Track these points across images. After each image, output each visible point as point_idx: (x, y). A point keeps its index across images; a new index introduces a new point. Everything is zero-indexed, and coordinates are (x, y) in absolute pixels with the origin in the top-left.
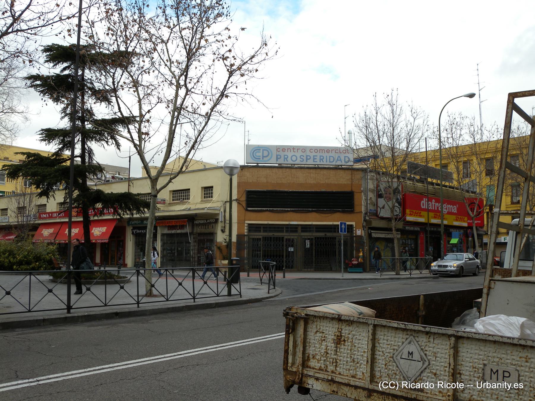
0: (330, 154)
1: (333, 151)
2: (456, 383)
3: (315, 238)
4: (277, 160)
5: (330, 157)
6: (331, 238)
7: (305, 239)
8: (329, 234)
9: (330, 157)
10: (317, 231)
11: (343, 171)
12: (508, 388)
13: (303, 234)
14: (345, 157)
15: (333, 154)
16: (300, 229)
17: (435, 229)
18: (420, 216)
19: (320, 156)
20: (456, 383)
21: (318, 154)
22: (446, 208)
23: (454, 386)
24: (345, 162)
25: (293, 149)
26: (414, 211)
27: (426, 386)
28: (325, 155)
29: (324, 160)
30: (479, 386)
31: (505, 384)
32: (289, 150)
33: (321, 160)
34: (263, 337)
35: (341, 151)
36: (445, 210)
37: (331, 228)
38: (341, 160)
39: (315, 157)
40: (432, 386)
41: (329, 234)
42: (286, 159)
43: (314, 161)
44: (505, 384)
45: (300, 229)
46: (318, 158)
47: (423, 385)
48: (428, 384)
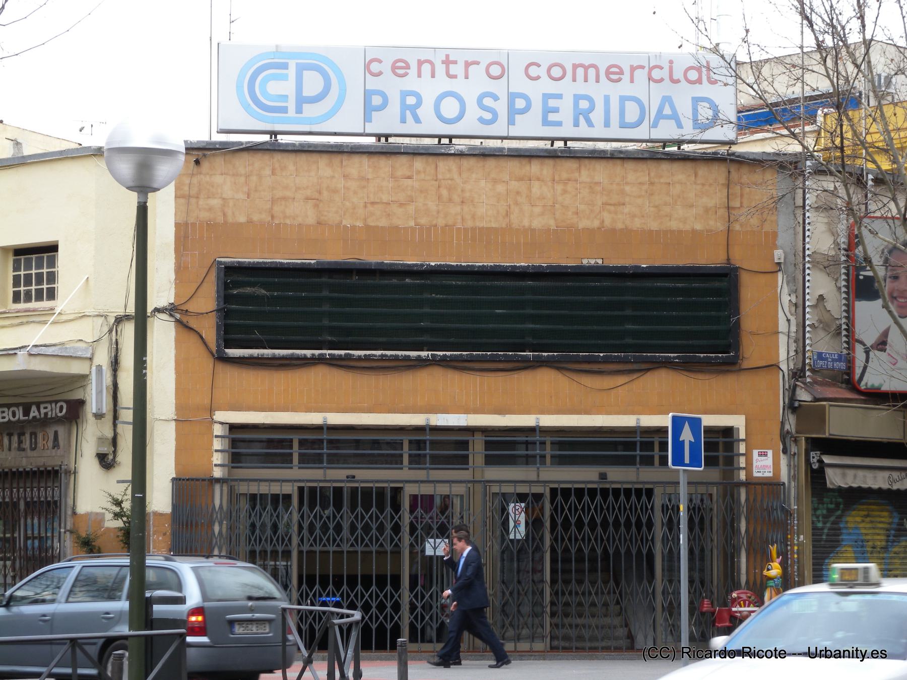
0: (625, 88)
4: (367, 118)
5: (623, 99)
9: (623, 99)
13: (495, 473)
14: (696, 101)
15: (639, 88)
16: (477, 449)
19: (577, 98)
21: (567, 88)
25: (447, 62)
28: (599, 90)
29: (597, 116)
32: (592, 72)
38: (675, 117)
39: (552, 103)
42: (413, 109)
43: (546, 122)
45: (477, 449)
46: (566, 108)
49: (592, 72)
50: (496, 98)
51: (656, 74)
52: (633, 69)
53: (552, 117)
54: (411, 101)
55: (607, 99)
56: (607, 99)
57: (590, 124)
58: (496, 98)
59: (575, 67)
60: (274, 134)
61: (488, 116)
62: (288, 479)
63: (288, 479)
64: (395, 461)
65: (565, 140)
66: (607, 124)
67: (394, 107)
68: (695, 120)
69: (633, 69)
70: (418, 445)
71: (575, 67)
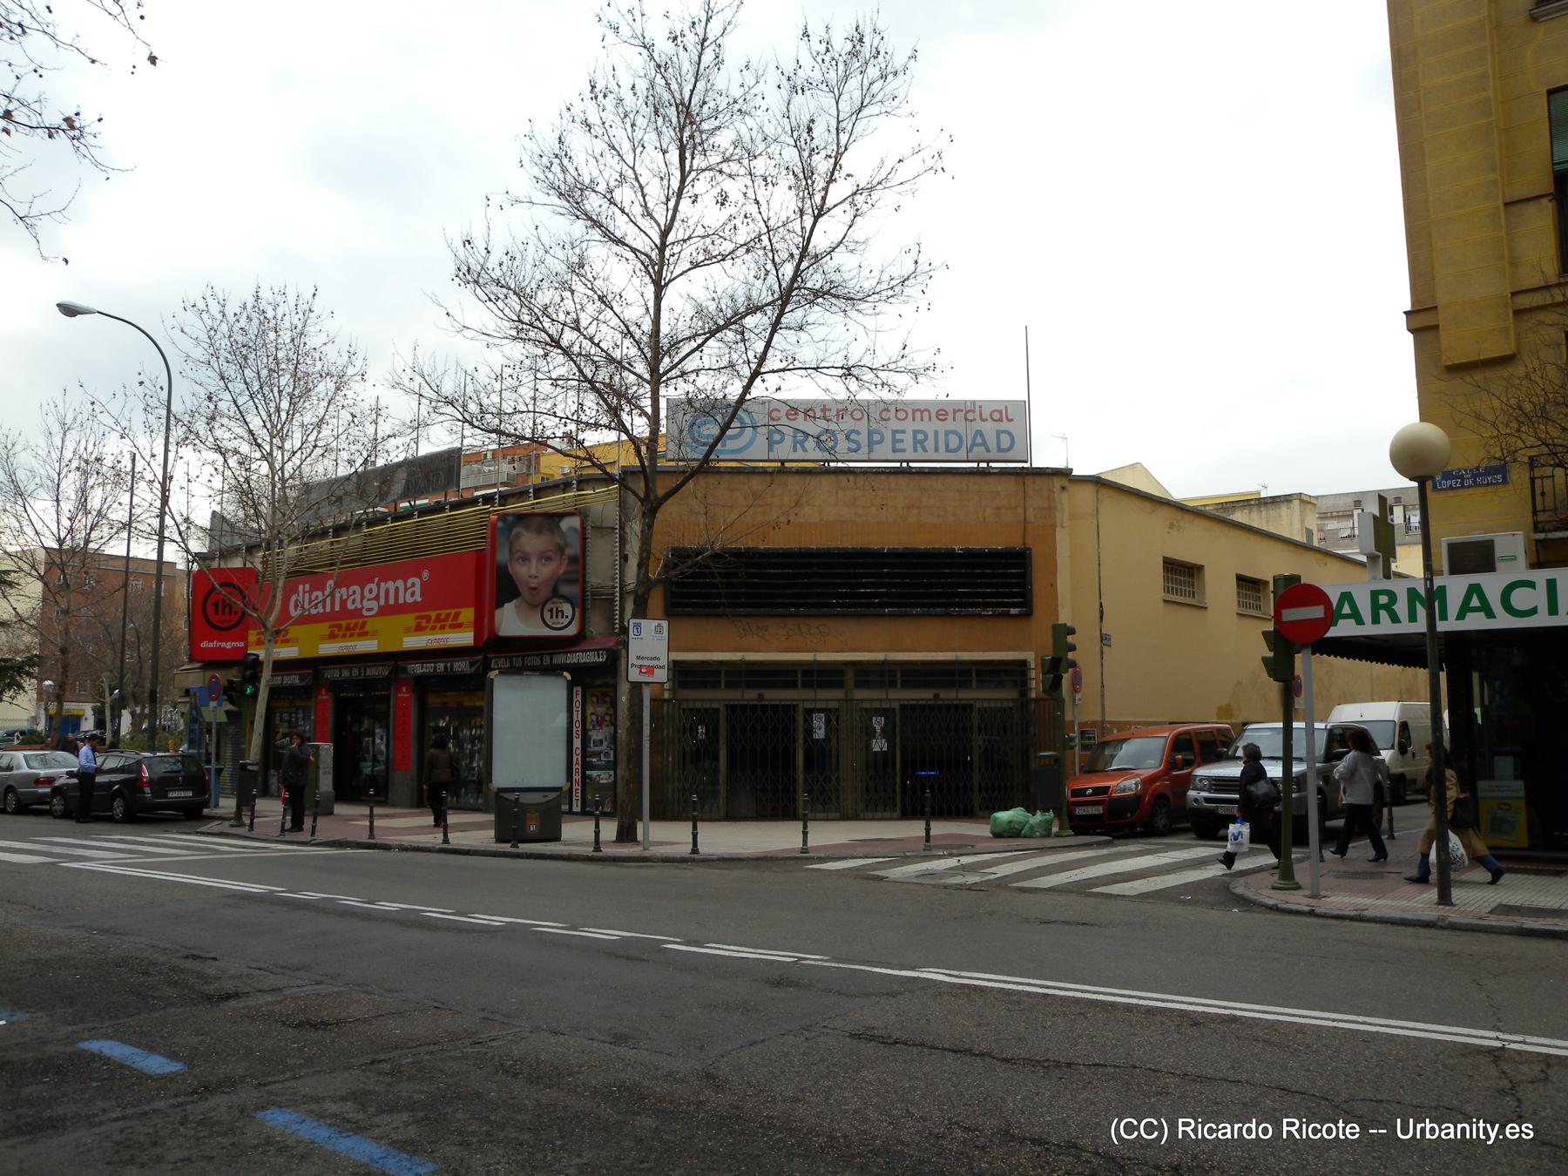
0: (949, 425)
1: (960, 416)
2: (1336, 1123)
3: (903, 707)
4: (770, 449)
5: (947, 433)
6: (957, 707)
7: (809, 712)
8: (948, 695)
9: (947, 433)
10: (906, 685)
11: (833, 477)
12: (1488, 1138)
13: (860, 694)
14: (999, 433)
15: (959, 425)
16: (850, 677)
17: (355, 673)
18: (364, 634)
19: (915, 432)
20: (1336, 1123)
21: (909, 426)
22: (365, 598)
23: (1329, 1131)
24: (1000, 450)
25: (824, 410)
26: (433, 614)
27: (1249, 1131)
28: (930, 427)
29: (930, 444)
30: (1405, 1132)
31: (1481, 1125)
32: (926, 414)
33: (919, 443)
34: (1050, 992)
35: (986, 415)
36: (374, 605)
37: (795, 673)
38: (984, 444)
39: (898, 436)
40: (1265, 1131)
41: (948, 695)
42: (922, 442)
43: (895, 450)
44: (1481, 1125)
45: (850, 677)
46: (908, 439)
47: (1240, 1129)
48: (1253, 1126)
49: (926, 414)
50: (858, 433)
51: (970, 416)
52: (955, 412)
53: (899, 446)
54: (920, 437)
55: (936, 433)
56: (936, 433)
57: (925, 450)
58: (858, 433)
59: (914, 411)
60: (783, 462)
61: (854, 446)
62: (718, 697)
63: (718, 697)
64: (791, 685)
65: (908, 462)
66: (937, 450)
67: (789, 440)
68: (947, 446)
69: (955, 412)
70: (979, 673)
71: (914, 411)
